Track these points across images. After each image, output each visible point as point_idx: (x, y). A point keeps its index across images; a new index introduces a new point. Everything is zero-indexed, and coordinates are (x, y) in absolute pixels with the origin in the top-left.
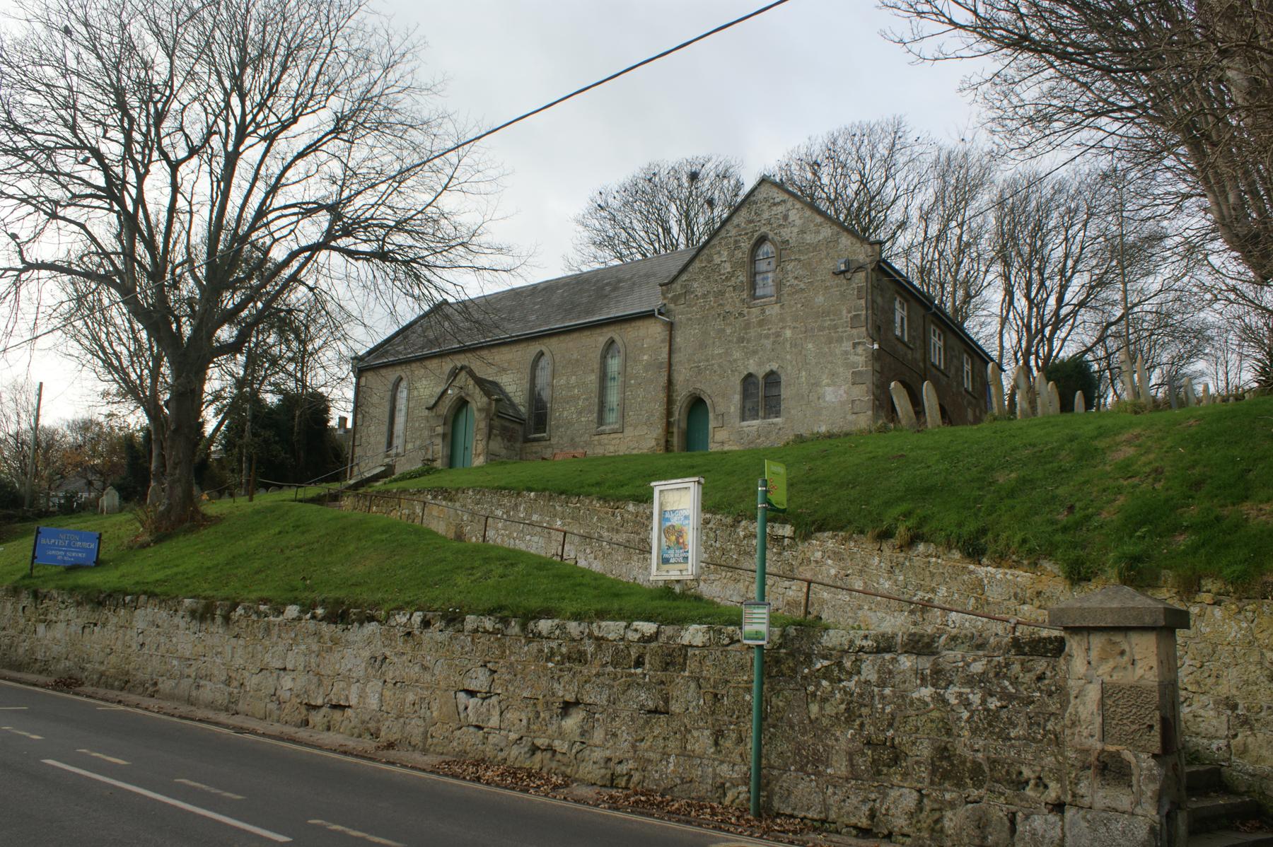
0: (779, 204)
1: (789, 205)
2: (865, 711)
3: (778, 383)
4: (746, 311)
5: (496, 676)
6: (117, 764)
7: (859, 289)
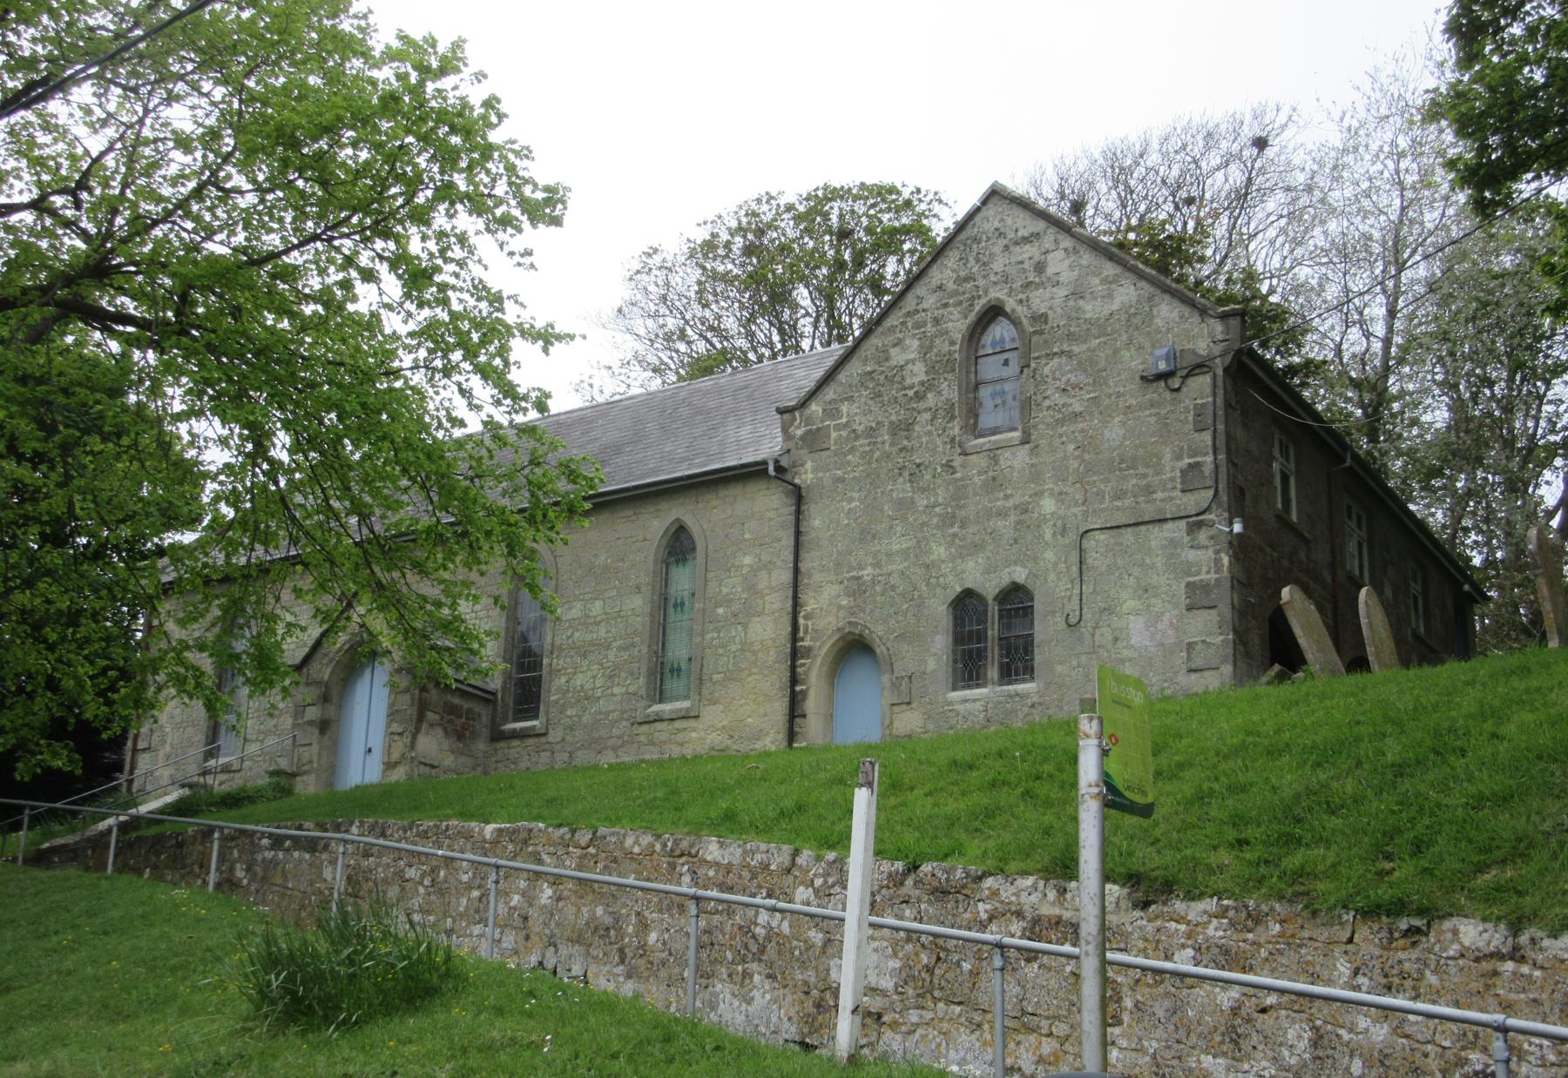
0: (1026, 240)
1: (1048, 242)
3: (1028, 612)
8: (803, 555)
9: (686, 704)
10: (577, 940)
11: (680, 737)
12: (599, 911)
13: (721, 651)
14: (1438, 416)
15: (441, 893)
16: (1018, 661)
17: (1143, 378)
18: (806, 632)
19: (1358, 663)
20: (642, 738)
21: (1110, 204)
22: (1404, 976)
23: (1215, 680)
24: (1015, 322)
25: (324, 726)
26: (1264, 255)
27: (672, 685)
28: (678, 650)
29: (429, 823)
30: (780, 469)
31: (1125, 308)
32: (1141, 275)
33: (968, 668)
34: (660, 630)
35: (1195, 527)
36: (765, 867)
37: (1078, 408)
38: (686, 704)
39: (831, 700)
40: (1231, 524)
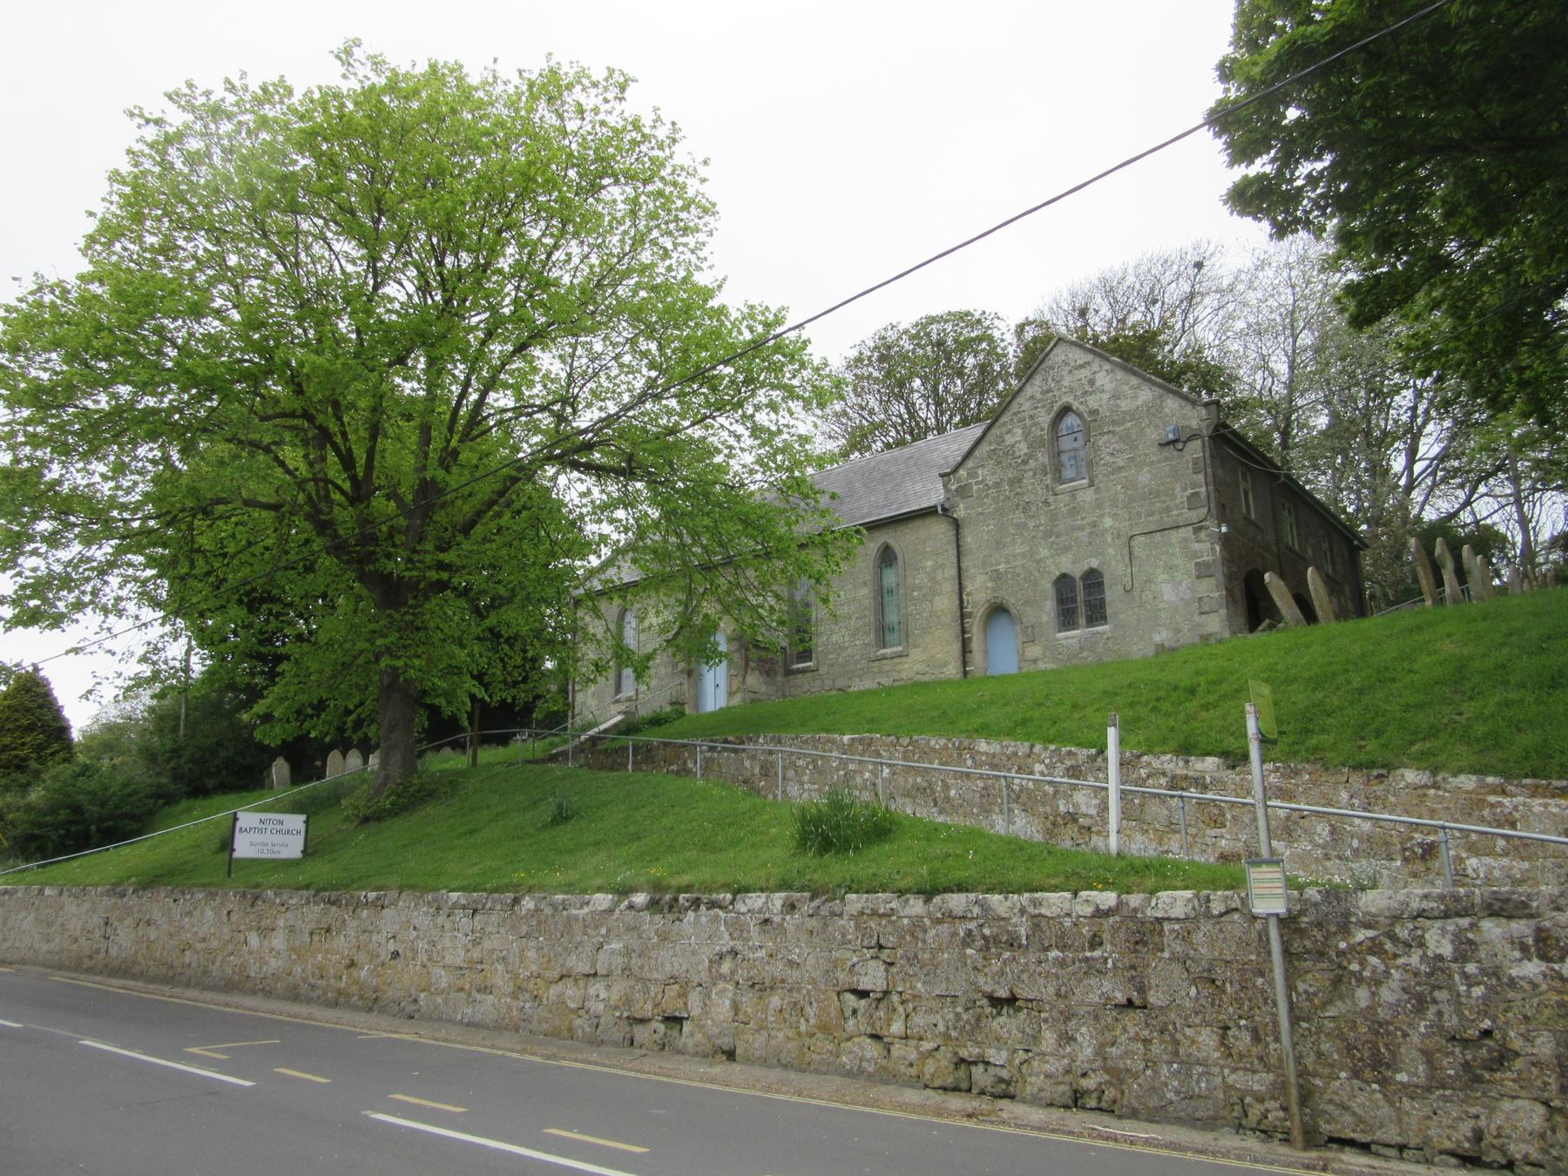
0: (1082, 366)
1: (1095, 367)
2: (1442, 995)
3: (1100, 585)
4: (1051, 499)
5: (894, 970)
6: (559, 1128)
7: (1195, 462)
8: (963, 559)
9: (900, 648)
10: (908, 795)
12: (919, 780)
14: (1322, 421)
15: (819, 772)
16: (1097, 614)
17: (1165, 445)
19: (1310, 616)
21: (1105, 311)
22: (1377, 798)
23: (1216, 623)
24: (1080, 415)
25: (690, 673)
26: (1205, 334)
27: (890, 637)
28: (892, 618)
29: (806, 736)
30: (944, 509)
31: (1145, 403)
32: (1154, 383)
33: (1067, 619)
34: (881, 608)
35: (1197, 530)
36: (1015, 754)
37: (1121, 464)
38: (900, 648)
39: (986, 642)
40: (1219, 527)
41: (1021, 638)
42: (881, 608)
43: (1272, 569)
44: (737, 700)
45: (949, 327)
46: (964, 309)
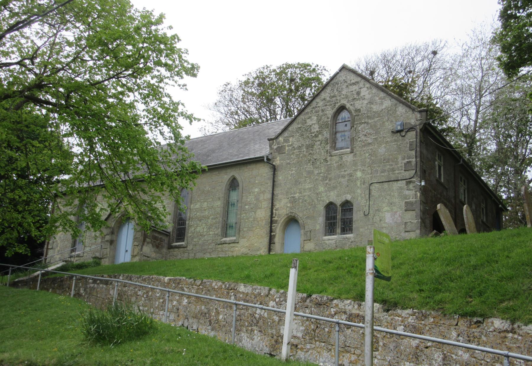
0: (354, 84)
1: (361, 85)
3: (351, 210)
8: (276, 189)
9: (234, 238)
10: (195, 317)
11: (232, 249)
12: (203, 307)
13: (246, 220)
14: (492, 147)
15: (150, 300)
17: (392, 132)
18: (276, 215)
19: (462, 231)
20: (219, 249)
21: (383, 72)
22: (474, 337)
24: (350, 112)
25: (112, 242)
26: (435, 91)
27: (230, 232)
28: (232, 220)
30: (268, 159)
31: (386, 108)
32: (393, 97)
33: (330, 229)
34: (226, 213)
35: (409, 183)
36: (259, 294)
37: (370, 141)
38: (234, 238)
39: (283, 239)
40: (421, 182)
41: (303, 238)
42: (226, 213)
43: (443, 202)
44: (136, 259)
45: (298, 71)
46: (307, 62)
